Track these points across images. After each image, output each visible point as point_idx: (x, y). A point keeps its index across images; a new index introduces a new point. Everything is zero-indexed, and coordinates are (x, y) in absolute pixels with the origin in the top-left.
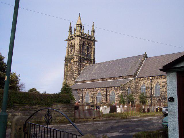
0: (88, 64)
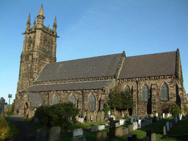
0: (48, 63)
